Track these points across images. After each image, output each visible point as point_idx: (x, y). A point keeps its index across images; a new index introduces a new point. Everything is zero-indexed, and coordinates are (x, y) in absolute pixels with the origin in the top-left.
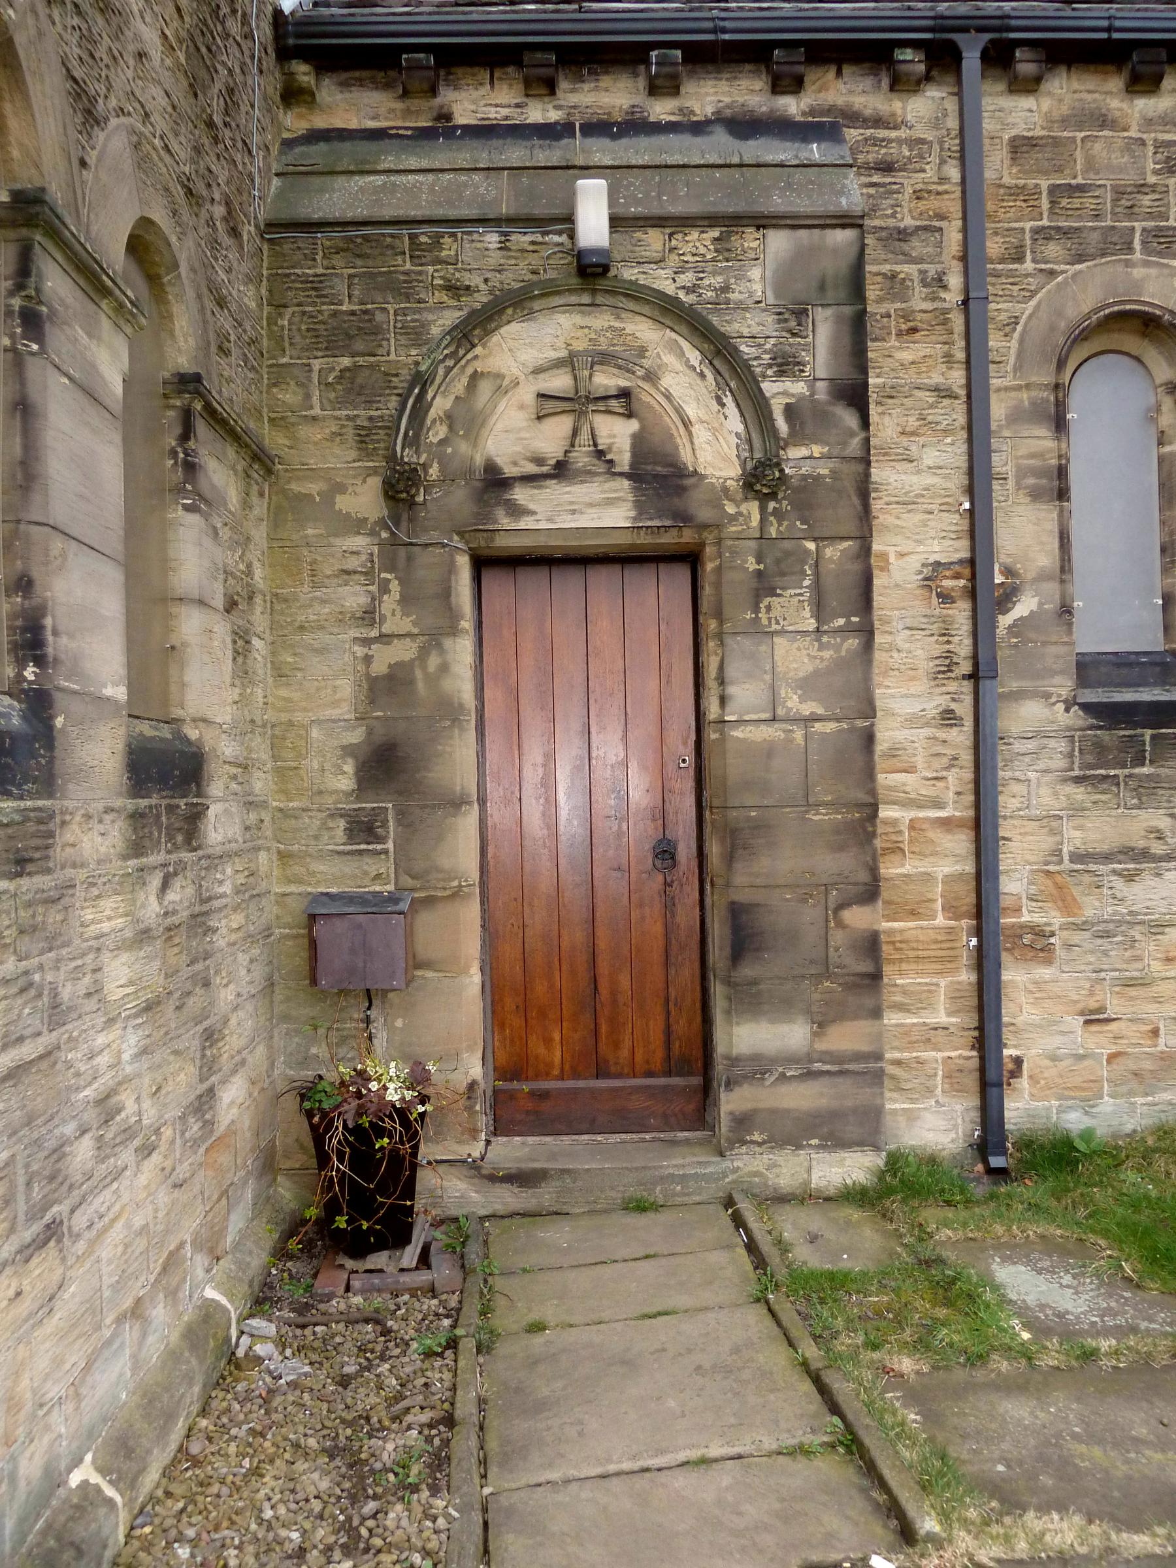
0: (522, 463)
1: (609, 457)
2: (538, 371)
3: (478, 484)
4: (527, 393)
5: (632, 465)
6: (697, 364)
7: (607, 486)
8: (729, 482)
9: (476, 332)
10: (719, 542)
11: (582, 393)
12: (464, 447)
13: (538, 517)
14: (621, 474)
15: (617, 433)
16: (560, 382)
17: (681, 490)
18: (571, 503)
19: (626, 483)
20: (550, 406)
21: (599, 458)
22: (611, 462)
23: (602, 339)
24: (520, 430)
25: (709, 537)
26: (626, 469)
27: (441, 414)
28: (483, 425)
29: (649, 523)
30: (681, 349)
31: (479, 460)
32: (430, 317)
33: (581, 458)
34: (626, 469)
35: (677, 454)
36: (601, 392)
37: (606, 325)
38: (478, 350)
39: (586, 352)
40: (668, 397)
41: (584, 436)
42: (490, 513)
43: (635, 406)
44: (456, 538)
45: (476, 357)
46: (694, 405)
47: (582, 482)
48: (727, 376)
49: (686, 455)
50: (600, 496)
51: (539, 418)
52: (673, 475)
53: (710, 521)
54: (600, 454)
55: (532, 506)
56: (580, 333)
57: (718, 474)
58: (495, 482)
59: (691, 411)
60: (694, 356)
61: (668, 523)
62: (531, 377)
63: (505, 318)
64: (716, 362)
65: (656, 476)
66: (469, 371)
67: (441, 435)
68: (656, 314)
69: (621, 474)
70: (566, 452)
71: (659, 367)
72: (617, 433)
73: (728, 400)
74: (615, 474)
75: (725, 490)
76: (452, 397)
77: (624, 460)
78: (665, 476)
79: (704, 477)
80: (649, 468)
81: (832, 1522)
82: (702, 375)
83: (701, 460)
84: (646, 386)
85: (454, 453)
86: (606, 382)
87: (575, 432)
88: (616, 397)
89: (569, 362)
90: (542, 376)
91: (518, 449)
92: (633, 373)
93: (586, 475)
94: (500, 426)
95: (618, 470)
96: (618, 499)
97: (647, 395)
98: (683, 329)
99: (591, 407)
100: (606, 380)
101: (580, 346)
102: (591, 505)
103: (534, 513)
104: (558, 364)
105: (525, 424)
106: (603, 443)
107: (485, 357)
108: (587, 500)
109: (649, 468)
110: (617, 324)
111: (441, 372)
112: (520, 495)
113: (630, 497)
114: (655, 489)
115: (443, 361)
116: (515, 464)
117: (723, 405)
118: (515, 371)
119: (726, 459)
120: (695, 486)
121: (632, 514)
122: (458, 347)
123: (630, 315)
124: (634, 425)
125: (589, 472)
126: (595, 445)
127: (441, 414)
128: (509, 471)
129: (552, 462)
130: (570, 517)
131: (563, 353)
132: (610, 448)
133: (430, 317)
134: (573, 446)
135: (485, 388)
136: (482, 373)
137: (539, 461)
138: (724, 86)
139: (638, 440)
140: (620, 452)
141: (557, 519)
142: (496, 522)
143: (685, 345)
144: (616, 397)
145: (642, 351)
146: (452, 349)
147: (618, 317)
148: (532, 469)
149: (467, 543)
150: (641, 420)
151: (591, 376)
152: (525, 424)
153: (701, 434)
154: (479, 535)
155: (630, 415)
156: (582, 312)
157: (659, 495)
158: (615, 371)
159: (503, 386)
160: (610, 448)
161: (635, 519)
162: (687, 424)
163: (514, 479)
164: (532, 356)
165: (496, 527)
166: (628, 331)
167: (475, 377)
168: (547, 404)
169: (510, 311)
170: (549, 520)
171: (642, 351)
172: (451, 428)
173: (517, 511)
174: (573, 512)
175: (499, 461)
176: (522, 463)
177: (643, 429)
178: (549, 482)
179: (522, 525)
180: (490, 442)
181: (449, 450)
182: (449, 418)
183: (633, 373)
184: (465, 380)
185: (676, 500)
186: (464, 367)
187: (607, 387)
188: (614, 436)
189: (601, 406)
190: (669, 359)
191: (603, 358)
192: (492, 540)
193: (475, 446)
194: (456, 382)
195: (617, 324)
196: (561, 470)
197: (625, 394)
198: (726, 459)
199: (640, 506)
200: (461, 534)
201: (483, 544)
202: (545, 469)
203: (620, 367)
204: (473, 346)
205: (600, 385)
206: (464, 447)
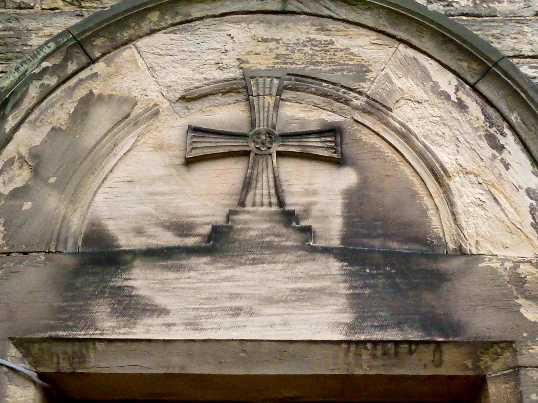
0: (153, 230)
1: (304, 223)
2: (189, 98)
3: (69, 261)
4: (172, 129)
5: (345, 239)
6: (451, 90)
7: (300, 269)
8: (523, 269)
9: (98, 42)
10: (515, 372)
11: (262, 127)
12: (52, 202)
13: (169, 319)
14: (327, 251)
15: (321, 192)
16: (228, 114)
17: (437, 280)
18: (233, 296)
19: (335, 266)
20: (207, 145)
21: (288, 224)
22: (308, 230)
23: (297, 55)
24: (154, 181)
25: (495, 367)
26: (336, 242)
27: (24, 151)
28: (92, 170)
29: (378, 336)
30: (423, 69)
31: (77, 224)
32: (33, 25)
33: (256, 222)
34: (336, 242)
35: (426, 224)
36: (294, 128)
37: (303, 37)
38: (99, 67)
39: (269, 73)
40: (406, 135)
41: (263, 188)
42: (83, 309)
43: (350, 150)
44: (13, 351)
45: (95, 75)
46: (452, 147)
47: (255, 262)
48: (502, 105)
49: (440, 225)
50: (285, 287)
51: (189, 162)
52: (424, 255)
53: (496, 335)
54: (289, 217)
55: (161, 300)
56: (261, 48)
57: (502, 253)
58: (101, 258)
59: (445, 156)
60: (447, 82)
61: (414, 335)
62: (179, 107)
63: (145, 26)
64: (482, 87)
65: (390, 256)
66: (81, 92)
67: (19, 183)
68: (383, 24)
69: (327, 251)
70: (231, 213)
71: (390, 93)
72: (321, 192)
73: (509, 140)
74: (314, 250)
75: (519, 281)
76: (47, 129)
77: (331, 228)
78: (406, 257)
79: (479, 257)
80: (377, 243)
81: (126, 85)
82: (461, 106)
83: (469, 231)
84: (367, 120)
85: (35, 210)
86: (302, 115)
87: (248, 184)
88: (319, 133)
89: (241, 88)
90: (197, 105)
91: (149, 209)
92: (346, 102)
93: (262, 250)
94: (120, 173)
95: (320, 243)
96: (321, 291)
97: (366, 137)
98: (426, 44)
99: (276, 147)
100: (301, 113)
101: (260, 63)
102: (269, 301)
103: (162, 311)
104: (227, 89)
105: (162, 172)
106: (294, 201)
107: (110, 76)
108: (263, 291)
109: (377, 243)
110: (321, 37)
111: (34, 91)
112: (142, 280)
113: (343, 288)
114: (388, 275)
115: (39, 76)
116: (140, 232)
117: (500, 148)
118: (154, 95)
119: (514, 229)
120: (462, 273)
121: (347, 317)
122: (67, 59)
123: (341, 26)
124: (348, 177)
125: (269, 246)
126: (281, 203)
127: (24, 151)
128: (127, 241)
129: (206, 230)
130: (228, 321)
131: (236, 73)
132: (307, 211)
133: (33, 25)
134: (242, 203)
135: (101, 119)
136: (101, 97)
137: (182, 228)
138: (477, 97)
139: (358, 206)
140: (325, 217)
141: (206, 324)
142: (91, 324)
143: (431, 66)
144: (319, 133)
145: (362, 71)
146: (56, 60)
147: (322, 29)
148: (169, 239)
149: (35, 363)
150: (360, 170)
151: (277, 107)
152: (162, 172)
153: (465, 192)
154: (58, 348)
155: (339, 162)
156: (269, 22)
157: (396, 287)
158: (317, 99)
159: (132, 116)
160: (307, 211)
161: (352, 327)
162: (439, 175)
163: (135, 254)
164: (184, 76)
165: (91, 334)
166: (338, 46)
167: (88, 101)
168: (202, 149)
169: (154, 16)
170: (192, 324)
171: (362, 71)
172: (35, 171)
173: (131, 307)
174: (236, 312)
175: (112, 227)
176: (153, 230)
177: (364, 182)
178: (194, 261)
179: (139, 332)
180: (99, 197)
181: (27, 206)
182: (36, 161)
183: (346, 102)
184: (70, 107)
185: (428, 297)
186: (73, 88)
187: (303, 121)
188: (315, 193)
189: (293, 147)
190: (405, 83)
191: (298, 82)
192: (83, 360)
193: (73, 200)
194: (56, 109)
195: (321, 37)
196: (219, 242)
197: (332, 131)
198: (514, 229)
199: (356, 301)
200: (23, 344)
201: (65, 367)
202: (190, 241)
203: (325, 95)
204: (93, 61)
205: (293, 119)
206: (52, 202)
